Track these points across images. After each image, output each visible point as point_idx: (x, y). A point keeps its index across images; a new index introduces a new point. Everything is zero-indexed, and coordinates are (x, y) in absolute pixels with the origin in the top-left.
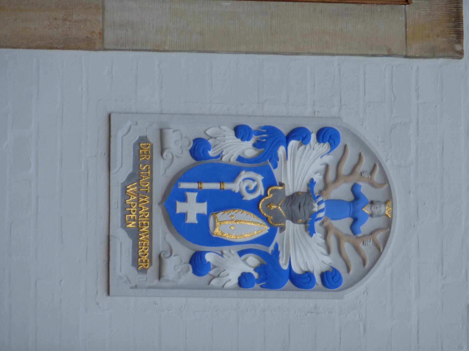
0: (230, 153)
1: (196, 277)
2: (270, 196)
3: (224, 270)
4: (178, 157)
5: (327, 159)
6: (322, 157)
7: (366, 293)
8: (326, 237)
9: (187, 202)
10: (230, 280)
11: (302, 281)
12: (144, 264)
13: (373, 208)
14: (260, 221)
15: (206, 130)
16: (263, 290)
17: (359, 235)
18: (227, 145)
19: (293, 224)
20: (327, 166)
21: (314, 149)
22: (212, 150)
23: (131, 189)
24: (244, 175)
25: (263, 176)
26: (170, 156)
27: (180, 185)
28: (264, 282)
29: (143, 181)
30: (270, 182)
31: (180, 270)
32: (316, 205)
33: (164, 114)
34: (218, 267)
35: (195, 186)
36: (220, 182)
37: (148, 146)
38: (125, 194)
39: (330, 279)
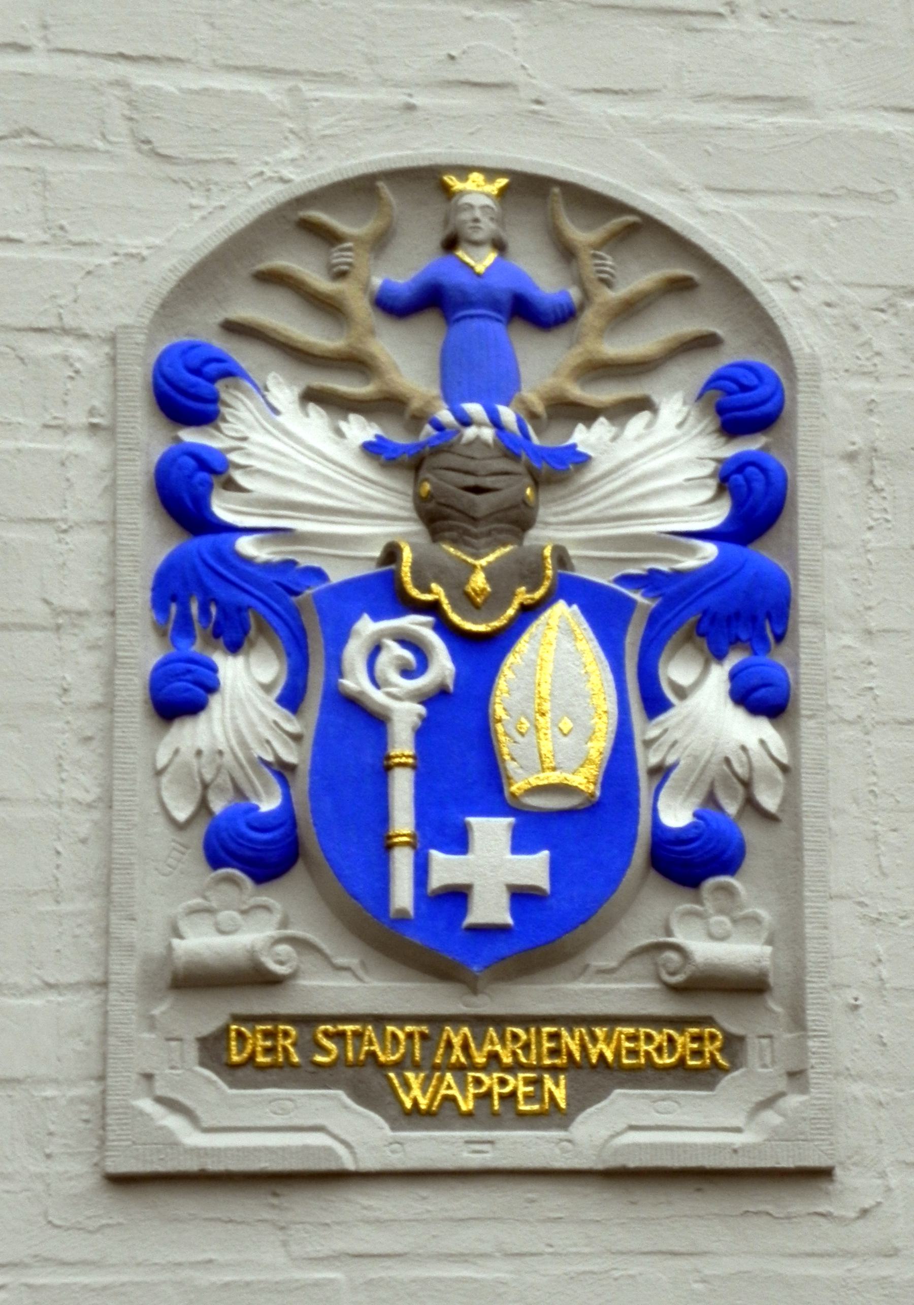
0: (267, 734)
1: (750, 863)
2: (438, 592)
3: (727, 761)
4: (284, 924)
5: (283, 392)
6: (276, 411)
7: (796, 283)
8: (588, 414)
9: (469, 887)
10: (762, 742)
11: (756, 503)
12: (708, 1048)
13: (478, 236)
14: (535, 628)
15: (172, 821)
16: (796, 630)
17: (574, 294)
18: (234, 742)
19: (537, 525)
20: (310, 396)
21: (244, 439)
22: (254, 802)
23: (416, 1092)
24: (355, 681)
25: (357, 617)
26: (284, 949)
27: (403, 911)
28: (763, 629)
29: (384, 1049)
30: (384, 591)
31: (725, 919)
32: (470, 433)
33: (106, 973)
34: (712, 785)
35: (402, 863)
36: (389, 768)
37: (240, 1034)
38: (442, 1114)
39: (746, 406)
